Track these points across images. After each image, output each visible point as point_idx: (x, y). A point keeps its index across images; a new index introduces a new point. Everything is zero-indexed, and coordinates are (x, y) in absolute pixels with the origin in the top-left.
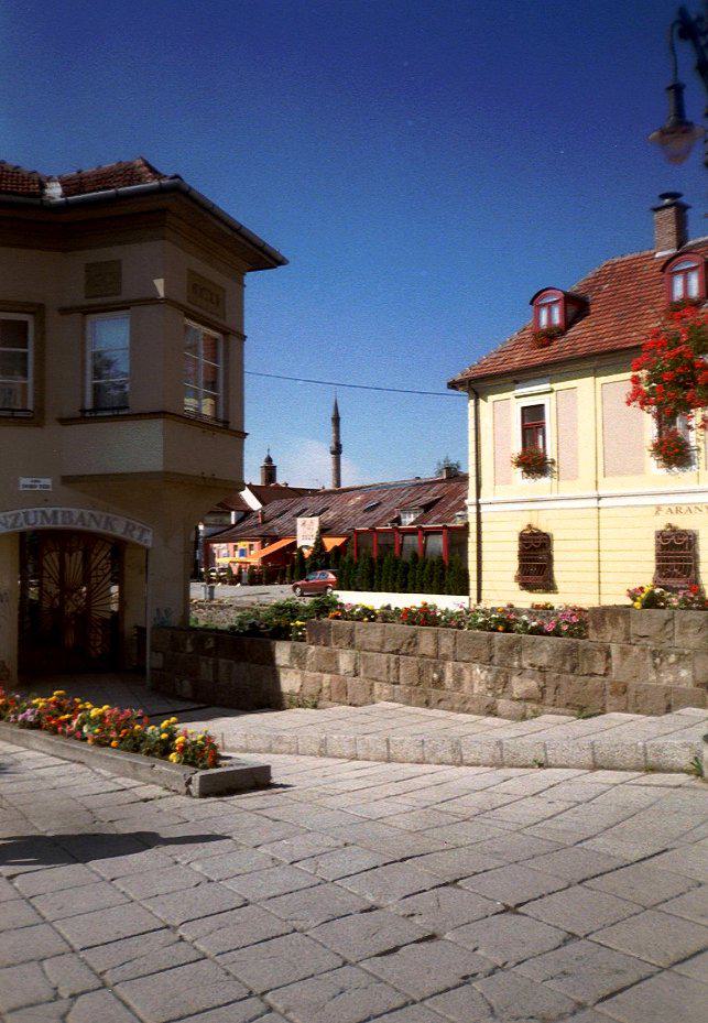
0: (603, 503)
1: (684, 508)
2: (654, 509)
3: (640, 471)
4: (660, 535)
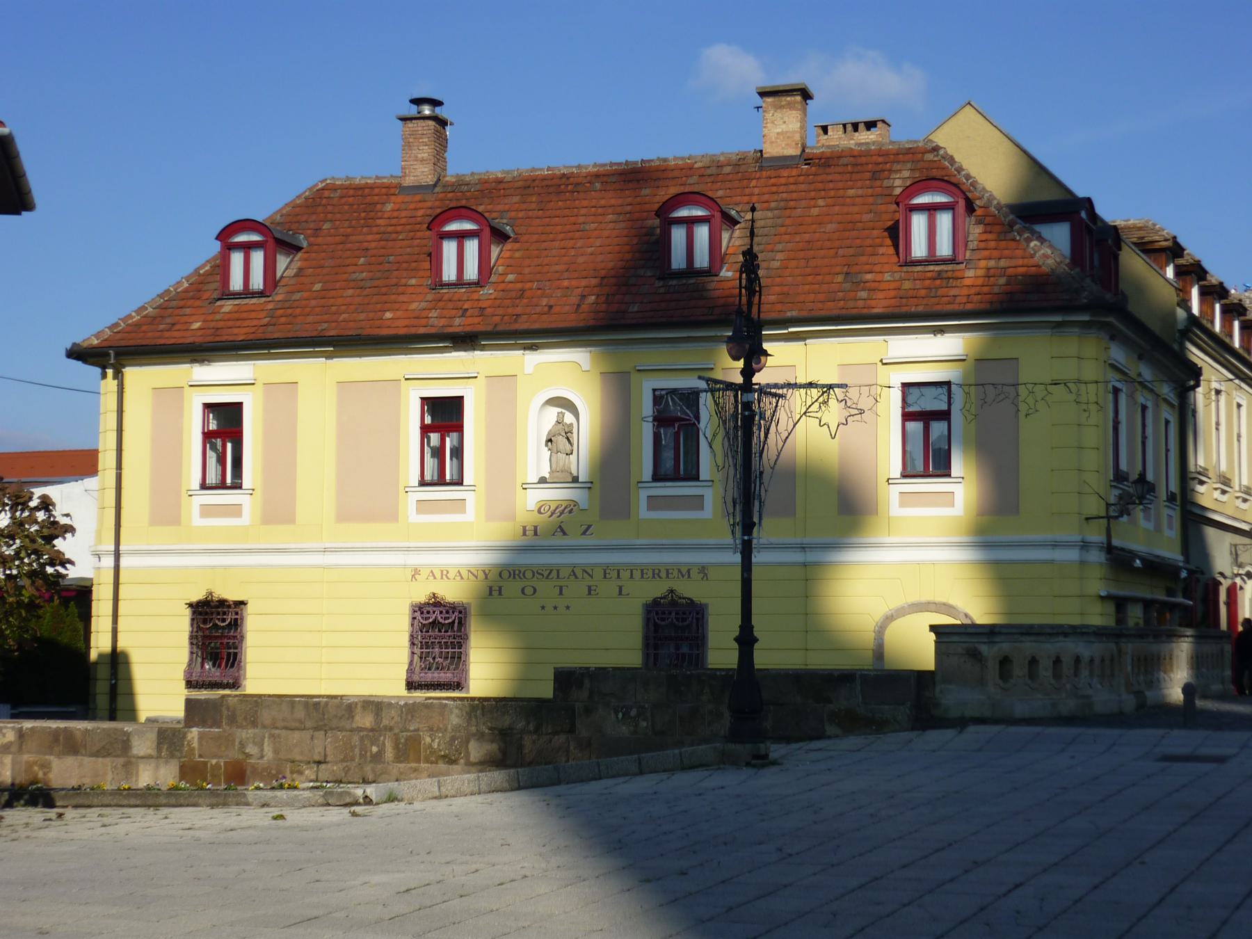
1: (565, 572)
3: (392, 515)
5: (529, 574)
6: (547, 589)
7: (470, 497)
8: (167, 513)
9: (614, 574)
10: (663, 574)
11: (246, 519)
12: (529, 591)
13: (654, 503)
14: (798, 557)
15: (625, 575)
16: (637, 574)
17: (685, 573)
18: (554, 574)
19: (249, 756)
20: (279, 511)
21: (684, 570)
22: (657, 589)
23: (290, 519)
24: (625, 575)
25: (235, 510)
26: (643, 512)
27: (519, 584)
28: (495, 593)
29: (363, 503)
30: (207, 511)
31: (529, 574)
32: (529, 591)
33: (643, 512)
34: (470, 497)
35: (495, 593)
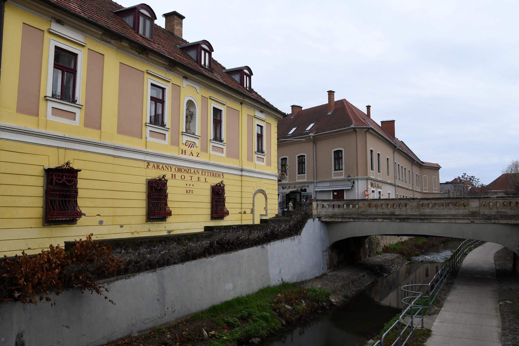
0: (244, 173)
1: (192, 171)
2: (146, 164)
6: (187, 176)
9: (204, 173)
12: (183, 177)
15: (207, 174)
18: (189, 171)
28: (174, 177)
32: (183, 177)
35: (174, 177)
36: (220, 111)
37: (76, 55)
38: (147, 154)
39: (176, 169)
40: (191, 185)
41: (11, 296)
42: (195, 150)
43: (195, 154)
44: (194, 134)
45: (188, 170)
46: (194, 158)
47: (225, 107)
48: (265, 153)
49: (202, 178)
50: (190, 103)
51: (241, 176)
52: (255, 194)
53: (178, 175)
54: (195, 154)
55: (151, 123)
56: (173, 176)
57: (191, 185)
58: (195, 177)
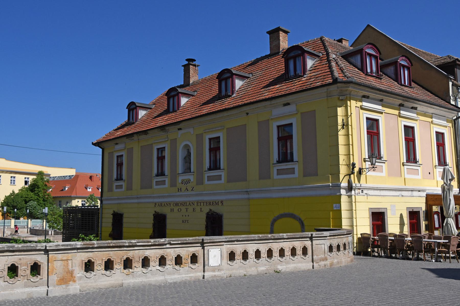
0: (251, 196)
1: (188, 204)
2: (154, 205)
3: (151, 187)
4: (208, 214)
5: (179, 205)
6: (184, 209)
7: (296, 167)
8: (265, 174)
9: (199, 204)
10: (212, 204)
11: (223, 180)
13: (280, 172)
14: (246, 196)
15: (202, 204)
16: (205, 204)
17: (161, 205)
19: (355, 190)
20: (129, 188)
21: (217, 202)
22: (206, 209)
23: (132, 189)
24: (202, 204)
25: (219, 177)
26: (275, 176)
27: (178, 207)
29: (146, 184)
30: (210, 178)
31: (179, 205)
33: (275, 176)
34: (296, 167)
36: (413, 128)
37: (377, 121)
38: (154, 197)
39: (174, 205)
40: (187, 216)
41: (41, 298)
42: (189, 186)
43: (190, 189)
44: (190, 172)
45: (183, 204)
46: (190, 193)
47: (417, 122)
48: (420, 163)
49: (198, 209)
50: (187, 148)
51: (249, 199)
52: (275, 220)
53: (176, 209)
54: (190, 189)
55: (407, 162)
56: (172, 210)
57: (187, 216)
58: (190, 209)
